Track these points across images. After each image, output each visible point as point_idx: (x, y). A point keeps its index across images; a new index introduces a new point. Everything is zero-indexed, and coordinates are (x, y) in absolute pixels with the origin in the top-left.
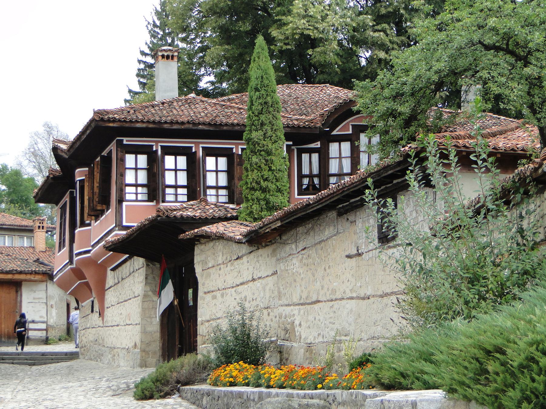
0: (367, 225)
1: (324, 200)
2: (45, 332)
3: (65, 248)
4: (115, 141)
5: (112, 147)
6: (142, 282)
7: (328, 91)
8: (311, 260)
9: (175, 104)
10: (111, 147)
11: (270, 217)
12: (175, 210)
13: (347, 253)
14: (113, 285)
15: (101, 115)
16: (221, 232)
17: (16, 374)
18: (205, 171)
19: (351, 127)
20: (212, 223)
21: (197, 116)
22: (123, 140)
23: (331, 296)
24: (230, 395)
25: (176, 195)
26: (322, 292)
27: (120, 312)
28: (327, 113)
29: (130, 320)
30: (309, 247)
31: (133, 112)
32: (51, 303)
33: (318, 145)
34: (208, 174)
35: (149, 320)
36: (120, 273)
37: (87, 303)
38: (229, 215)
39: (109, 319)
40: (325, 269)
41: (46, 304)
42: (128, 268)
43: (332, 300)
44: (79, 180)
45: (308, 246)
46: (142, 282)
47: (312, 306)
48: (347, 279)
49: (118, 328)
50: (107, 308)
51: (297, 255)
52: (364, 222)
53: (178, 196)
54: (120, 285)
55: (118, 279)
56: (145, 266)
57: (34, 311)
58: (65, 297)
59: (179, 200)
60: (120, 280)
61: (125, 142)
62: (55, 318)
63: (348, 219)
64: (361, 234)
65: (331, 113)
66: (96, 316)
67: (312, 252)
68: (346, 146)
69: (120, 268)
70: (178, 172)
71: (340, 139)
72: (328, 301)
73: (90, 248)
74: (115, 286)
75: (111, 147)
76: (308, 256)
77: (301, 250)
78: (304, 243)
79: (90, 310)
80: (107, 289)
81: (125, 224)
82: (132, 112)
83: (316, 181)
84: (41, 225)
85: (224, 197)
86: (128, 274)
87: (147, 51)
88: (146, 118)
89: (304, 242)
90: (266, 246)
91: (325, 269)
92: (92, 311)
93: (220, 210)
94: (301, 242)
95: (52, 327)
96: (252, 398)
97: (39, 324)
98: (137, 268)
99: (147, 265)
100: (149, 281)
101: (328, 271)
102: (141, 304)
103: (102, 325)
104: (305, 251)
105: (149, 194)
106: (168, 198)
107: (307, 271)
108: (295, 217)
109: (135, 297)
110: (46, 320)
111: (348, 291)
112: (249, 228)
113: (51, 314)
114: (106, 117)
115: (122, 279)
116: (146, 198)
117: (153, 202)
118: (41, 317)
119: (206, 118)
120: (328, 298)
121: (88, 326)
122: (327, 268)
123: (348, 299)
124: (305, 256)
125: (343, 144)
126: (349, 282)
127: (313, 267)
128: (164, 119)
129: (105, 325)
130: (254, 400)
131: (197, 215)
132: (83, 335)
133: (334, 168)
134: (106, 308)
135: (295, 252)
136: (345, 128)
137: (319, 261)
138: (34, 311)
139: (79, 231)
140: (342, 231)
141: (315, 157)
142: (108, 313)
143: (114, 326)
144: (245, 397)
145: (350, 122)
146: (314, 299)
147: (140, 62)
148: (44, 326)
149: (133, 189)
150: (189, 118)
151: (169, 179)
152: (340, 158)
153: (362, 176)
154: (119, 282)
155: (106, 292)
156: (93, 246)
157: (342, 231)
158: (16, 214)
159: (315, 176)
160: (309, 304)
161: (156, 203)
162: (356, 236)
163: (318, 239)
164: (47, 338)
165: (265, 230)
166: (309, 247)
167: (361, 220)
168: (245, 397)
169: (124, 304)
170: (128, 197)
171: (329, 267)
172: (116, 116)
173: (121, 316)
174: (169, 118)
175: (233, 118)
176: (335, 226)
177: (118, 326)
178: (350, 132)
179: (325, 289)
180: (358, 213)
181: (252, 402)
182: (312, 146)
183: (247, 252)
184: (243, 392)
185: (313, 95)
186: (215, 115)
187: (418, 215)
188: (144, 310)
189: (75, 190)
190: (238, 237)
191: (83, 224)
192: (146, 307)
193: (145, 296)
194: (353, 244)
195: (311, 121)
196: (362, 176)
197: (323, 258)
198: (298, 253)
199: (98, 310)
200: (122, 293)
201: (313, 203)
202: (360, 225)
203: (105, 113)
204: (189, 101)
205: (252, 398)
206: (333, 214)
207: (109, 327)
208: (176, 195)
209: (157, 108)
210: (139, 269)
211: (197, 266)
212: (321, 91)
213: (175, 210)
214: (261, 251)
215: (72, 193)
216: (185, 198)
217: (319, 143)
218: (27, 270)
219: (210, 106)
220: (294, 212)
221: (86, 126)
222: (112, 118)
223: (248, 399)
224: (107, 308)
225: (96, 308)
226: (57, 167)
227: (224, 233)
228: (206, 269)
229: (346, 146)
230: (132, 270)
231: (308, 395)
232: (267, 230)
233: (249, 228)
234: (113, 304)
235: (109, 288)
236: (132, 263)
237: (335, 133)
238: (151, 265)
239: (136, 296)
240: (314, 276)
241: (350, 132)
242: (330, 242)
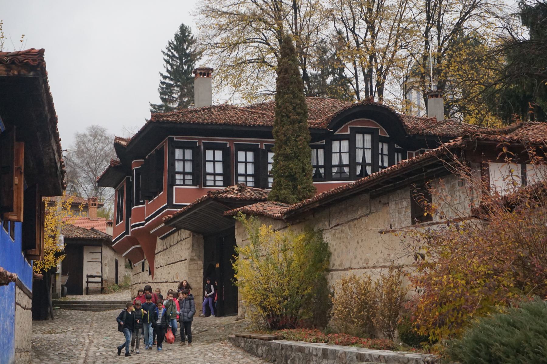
0: (400, 207)
1: (362, 186)
2: (100, 284)
3: (122, 221)
4: (167, 138)
5: (165, 143)
6: (189, 249)
7: (326, 102)
8: (344, 235)
9: (213, 110)
10: (163, 143)
11: (310, 199)
12: (222, 193)
13: (379, 229)
14: (161, 250)
15: (157, 118)
16: (261, 211)
17: (85, 320)
18: (237, 162)
19: (349, 129)
20: (252, 204)
21: (231, 120)
22: (173, 138)
23: (364, 264)
24: (289, 348)
25: (215, 181)
26: (355, 261)
27: (168, 272)
28: (331, 118)
29: (177, 278)
30: (342, 224)
31: (181, 116)
32: (105, 262)
33: (324, 143)
34: (239, 165)
35: (194, 279)
36: (168, 241)
37: (138, 265)
38: (263, 197)
39: (158, 277)
40: (358, 242)
41: (101, 262)
42: (176, 237)
43: (365, 268)
44: (135, 169)
45: (341, 223)
46: (189, 249)
47: (345, 272)
48: (380, 251)
49: (166, 284)
50: (157, 268)
51: (330, 230)
52: (396, 204)
53: (186, 180)
54: (168, 250)
55: (166, 246)
56: (191, 236)
57: (92, 268)
58: (115, 258)
59: (186, 183)
60: (168, 247)
61: (175, 139)
62: (108, 273)
63: (380, 202)
64: (394, 214)
65: (334, 118)
66: (146, 274)
67: (345, 228)
68: (345, 144)
69: (169, 238)
70: (248, 164)
71: (340, 138)
72: (361, 268)
73: (144, 222)
74: (164, 251)
75: (123, 183)
76: (341, 231)
77: (335, 226)
78: (337, 221)
79: (141, 269)
80: (157, 254)
81: (174, 203)
82: (181, 115)
83: (322, 171)
84: (94, 203)
85: (251, 183)
86: (176, 242)
87: (167, 74)
88: (192, 121)
89: (337, 219)
90: (300, 222)
91: (358, 242)
92: (143, 270)
93: (255, 193)
94: (334, 220)
95: (106, 281)
96: (314, 353)
97: (96, 278)
98: (184, 238)
99: (193, 236)
100: (195, 248)
101: (361, 244)
102: (187, 266)
103: (152, 281)
104: (339, 227)
105: (193, 180)
106: (208, 183)
107: (340, 243)
108: (333, 199)
109: (182, 261)
110: (101, 275)
111: (381, 260)
112: (288, 208)
113: (105, 271)
114: (161, 120)
115: (170, 246)
116: (191, 183)
117: (197, 186)
118: (97, 273)
119: (238, 121)
120: (361, 266)
121: (139, 282)
122: (360, 241)
123: (382, 267)
124: (337, 231)
125: (343, 142)
126: (383, 254)
127: (345, 240)
128: (206, 121)
129: (154, 281)
130: (316, 355)
131: (239, 196)
132: (135, 289)
133: (335, 160)
134: (155, 268)
135: (328, 227)
136: (345, 130)
137: (352, 235)
138: (92, 268)
139: (135, 208)
140: (374, 211)
141: (321, 152)
142: (157, 272)
143: (163, 282)
144: (307, 352)
145: (349, 125)
146: (347, 266)
147: (163, 83)
148: (99, 280)
149: (211, 178)
150: (225, 121)
151: (209, 168)
152: (340, 152)
153: (403, 166)
154: (167, 248)
155: (156, 256)
156: (147, 220)
157: (374, 211)
158: (509, 227)
159: (321, 167)
160: (341, 270)
161: (199, 187)
162: (389, 215)
163: (350, 217)
164: (103, 289)
165: (305, 209)
166: (342, 224)
167: (394, 203)
168: (307, 352)
169: (172, 267)
170: (178, 182)
171: (362, 240)
172: (168, 118)
173: (169, 275)
174: (210, 121)
175: (259, 121)
176: (367, 207)
177: (166, 282)
178: (349, 133)
179: (358, 259)
180: (391, 197)
181: (314, 357)
182: (319, 143)
183: (282, 227)
184: (304, 347)
185: (315, 105)
186: (244, 119)
187: (453, 199)
188: (190, 270)
189: (131, 177)
190: (277, 215)
191: (138, 203)
192: (192, 268)
193: (192, 260)
194: (386, 222)
195: (319, 124)
196: (403, 166)
197: (356, 233)
198: (331, 228)
199: (148, 269)
200: (170, 257)
201: (352, 188)
202: (393, 206)
203: (160, 117)
204: (223, 108)
205: (314, 353)
206: (366, 196)
207: (158, 283)
208: (215, 181)
209: (199, 113)
210: (186, 239)
211: (238, 237)
212: (321, 101)
213: (222, 193)
214: (295, 227)
215: (128, 179)
216: (221, 184)
217: (324, 141)
218: (87, 237)
219: (240, 112)
220: (333, 195)
221: (144, 126)
222: (166, 120)
223: (310, 354)
224: (157, 268)
225: (147, 267)
226: (118, 160)
227: (264, 212)
228: (245, 240)
229: (345, 144)
230: (179, 239)
231: (384, 357)
232: (306, 210)
233: (288, 208)
234: (162, 265)
235: (159, 253)
236: (180, 234)
237: (336, 133)
238: (197, 236)
239: (183, 259)
240: (347, 248)
241: (349, 133)
242: (363, 220)
